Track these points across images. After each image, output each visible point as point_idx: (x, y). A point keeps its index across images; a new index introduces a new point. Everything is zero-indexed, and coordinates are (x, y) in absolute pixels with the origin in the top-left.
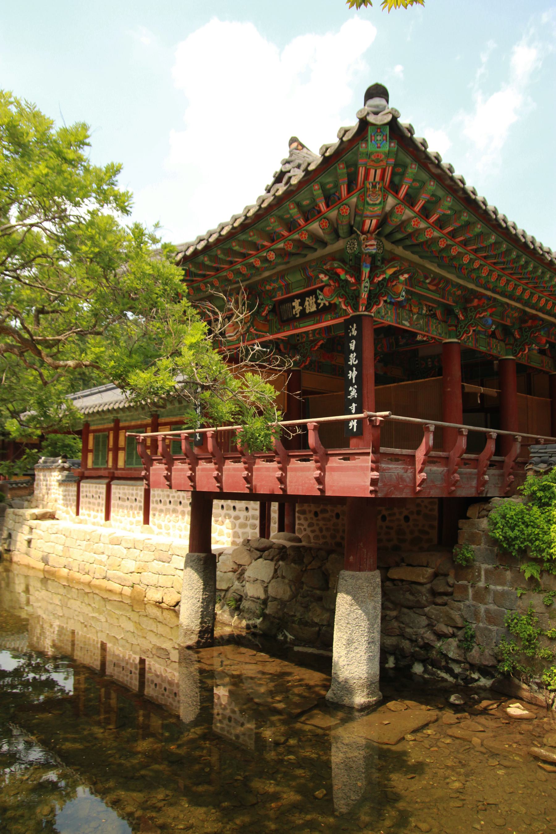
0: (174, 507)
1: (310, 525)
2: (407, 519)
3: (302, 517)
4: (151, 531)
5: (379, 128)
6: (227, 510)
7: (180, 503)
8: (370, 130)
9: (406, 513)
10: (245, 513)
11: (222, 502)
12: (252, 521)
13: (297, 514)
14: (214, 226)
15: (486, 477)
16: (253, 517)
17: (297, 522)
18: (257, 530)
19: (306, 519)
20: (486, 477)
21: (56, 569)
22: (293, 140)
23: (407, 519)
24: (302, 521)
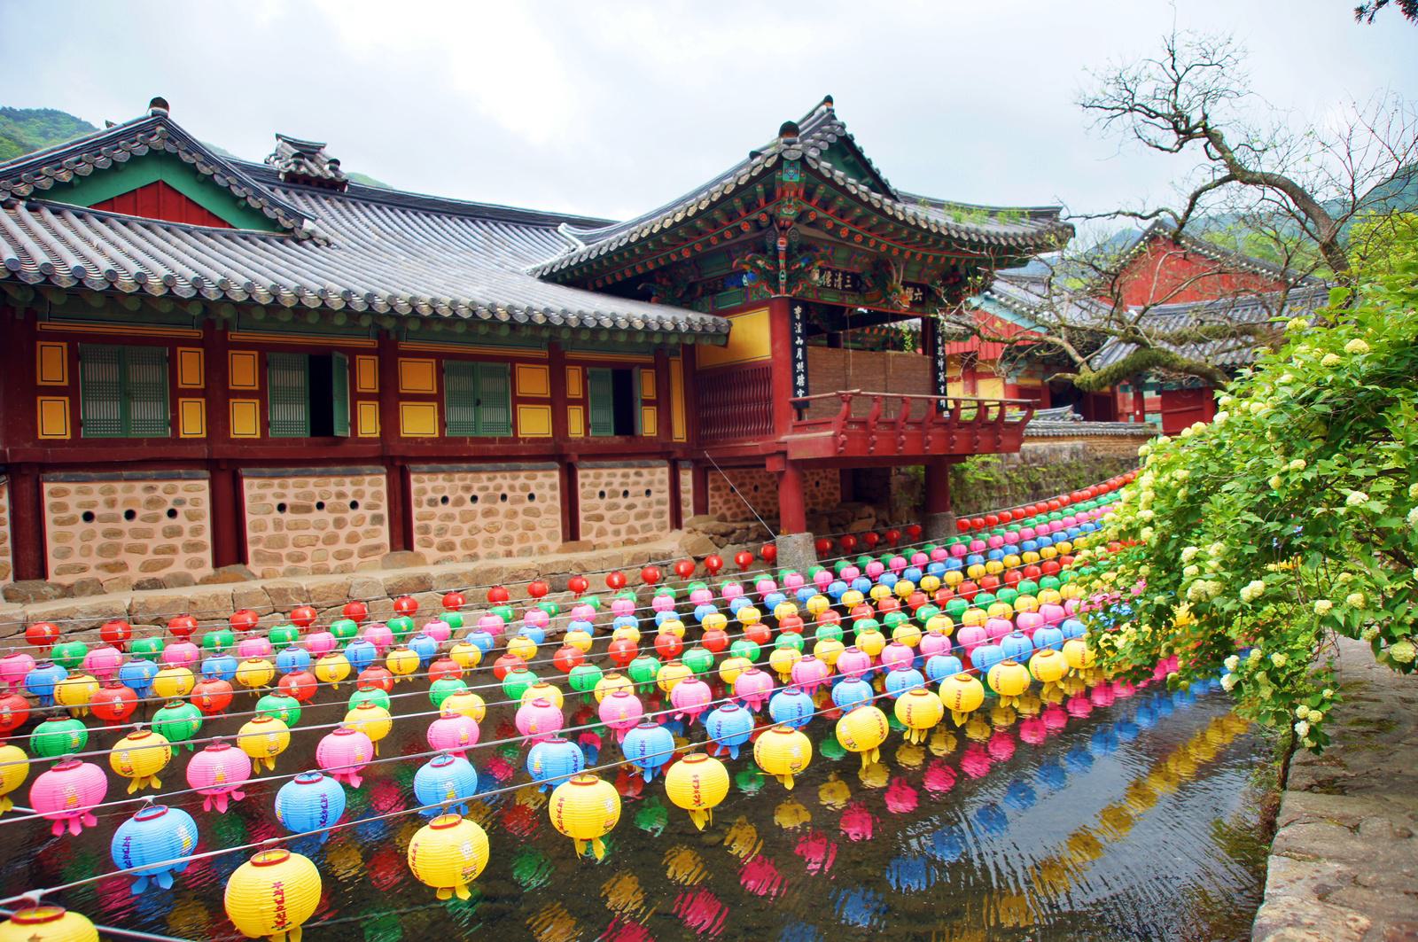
0: (487, 506)
1: (726, 502)
2: (817, 484)
3: (717, 494)
4: (420, 560)
5: (792, 164)
6: (611, 497)
7: (504, 497)
8: (785, 165)
9: (817, 478)
10: (645, 499)
11: (95, 493)
12: (656, 508)
13: (710, 492)
14: (216, 145)
15: (930, 437)
16: (659, 502)
17: (710, 501)
18: (385, 529)
19: (721, 496)
20: (930, 437)
21: (649, 715)
22: (158, 102)
23: (817, 484)
24: (717, 499)
